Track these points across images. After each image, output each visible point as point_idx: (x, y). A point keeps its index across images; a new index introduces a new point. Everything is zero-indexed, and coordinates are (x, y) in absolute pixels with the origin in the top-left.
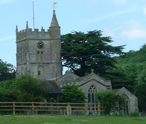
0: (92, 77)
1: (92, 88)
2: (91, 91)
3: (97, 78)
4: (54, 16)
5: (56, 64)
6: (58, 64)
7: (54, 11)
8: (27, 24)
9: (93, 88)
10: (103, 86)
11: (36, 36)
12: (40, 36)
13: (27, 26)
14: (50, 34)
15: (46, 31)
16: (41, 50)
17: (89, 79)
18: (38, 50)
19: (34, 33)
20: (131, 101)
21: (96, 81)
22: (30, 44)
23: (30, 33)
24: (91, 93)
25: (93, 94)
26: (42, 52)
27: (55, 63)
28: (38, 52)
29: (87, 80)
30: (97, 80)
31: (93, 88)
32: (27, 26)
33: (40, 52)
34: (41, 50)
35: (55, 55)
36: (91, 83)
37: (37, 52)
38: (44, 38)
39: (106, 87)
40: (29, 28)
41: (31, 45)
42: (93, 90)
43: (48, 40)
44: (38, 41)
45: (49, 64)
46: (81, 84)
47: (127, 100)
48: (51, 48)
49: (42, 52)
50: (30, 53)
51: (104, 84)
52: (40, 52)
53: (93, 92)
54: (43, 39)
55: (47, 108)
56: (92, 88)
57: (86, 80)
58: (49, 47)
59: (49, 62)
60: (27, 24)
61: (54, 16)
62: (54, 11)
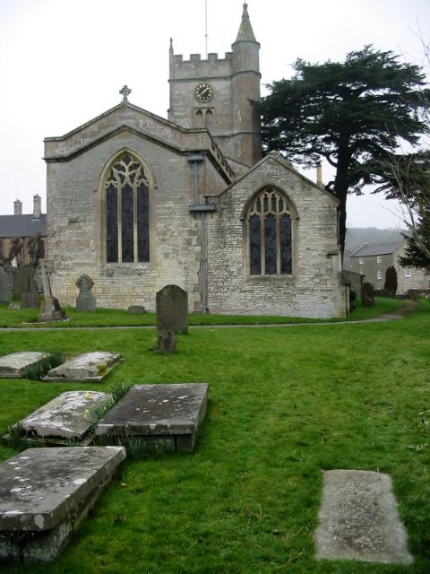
0: (122, 118)
1: (123, 163)
2: (123, 178)
3: (141, 122)
4: (245, 17)
5: (240, 137)
6: (246, 135)
7: (245, 6)
8: (171, 45)
9: (130, 164)
10: (169, 153)
11: (193, 72)
12: (205, 72)
13: (171, 50)
14: (231, 64)
15: (221, 56)
16: (206, 105)
17: (107, 126)
18: (197, 105)
19: (188, 65)
20: (301, 214)
21: (140, 134)
22: (177, 92)
23: (177, 65)
24: (119, 186)
25: (127, 189)
26: (209, 111)
27: (240, 133)
28: (200, 112)
29: (99, 132)
30: (141, 128)
31: (130, 164)
32: (171, 50)
33: (204, 111)
34: (206, 105)
35: (239, 113)
36: (117, 144)
37: (196, 111)
38: (215, 74)
39: (184, 160)
40: (175, 54)
41: (178, 95)
42: (127, 174)
43: (225, 78)
44: (194, 85)
45: (226, 140)
46: (73, 149)
47: (285, 211)
48: (232, 99)
49: (209, 111)
50: (176, 113)
51: (174, 143)
52: (204, 111)
53: (127, 180)
54: (210, 78)
55: (269, 232)
56: (123, 163)
57: (93, 134)
58: (227, 97)
59: (227, 133)
60: (171, 45)
61: (245, 17)
62: (245, 6)
